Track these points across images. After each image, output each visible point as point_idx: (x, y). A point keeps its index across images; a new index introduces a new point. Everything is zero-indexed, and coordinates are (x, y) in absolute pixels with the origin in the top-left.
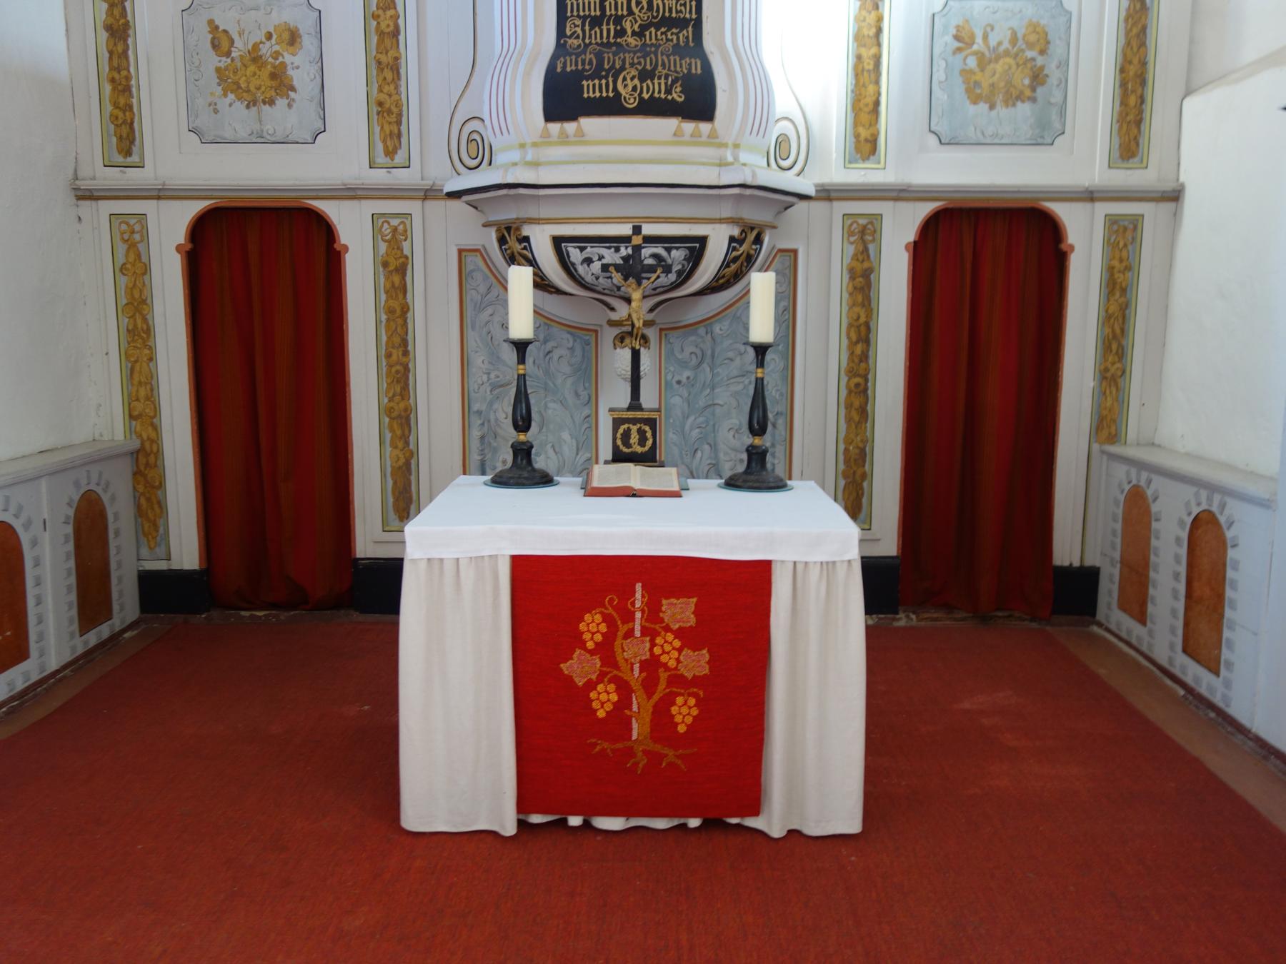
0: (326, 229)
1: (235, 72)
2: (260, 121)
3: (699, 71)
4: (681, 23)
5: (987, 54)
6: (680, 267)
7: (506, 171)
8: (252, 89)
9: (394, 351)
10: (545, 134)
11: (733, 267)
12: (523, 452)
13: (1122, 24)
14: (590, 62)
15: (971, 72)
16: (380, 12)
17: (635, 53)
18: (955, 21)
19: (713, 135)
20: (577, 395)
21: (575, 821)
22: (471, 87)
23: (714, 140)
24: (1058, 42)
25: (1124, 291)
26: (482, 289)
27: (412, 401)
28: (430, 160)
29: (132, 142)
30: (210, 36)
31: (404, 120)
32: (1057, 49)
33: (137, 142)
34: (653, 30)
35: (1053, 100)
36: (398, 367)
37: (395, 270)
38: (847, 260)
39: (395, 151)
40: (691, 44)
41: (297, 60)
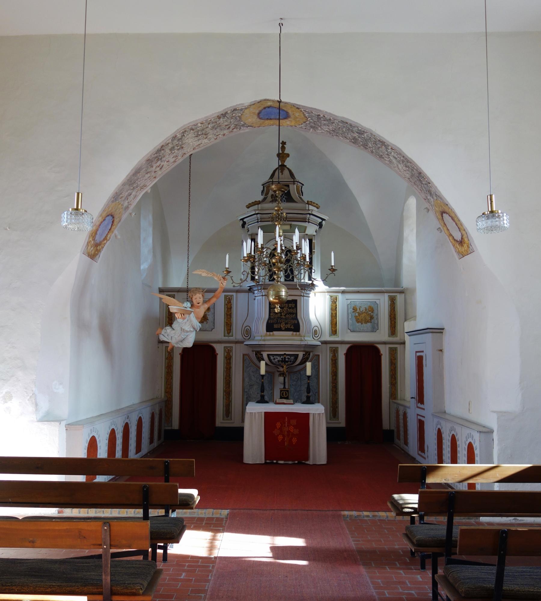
0: (213, 350)
4: (293, 314)
10: (266, 334)
12: (262, 397)
18: (353, 306)
19: (300, 334)
21: (275, 461)
23: (300, 335)
25: (394, 364)
28: (237, 335)
32: (375, 311)
37: (228, 359)
41: (209, 313)
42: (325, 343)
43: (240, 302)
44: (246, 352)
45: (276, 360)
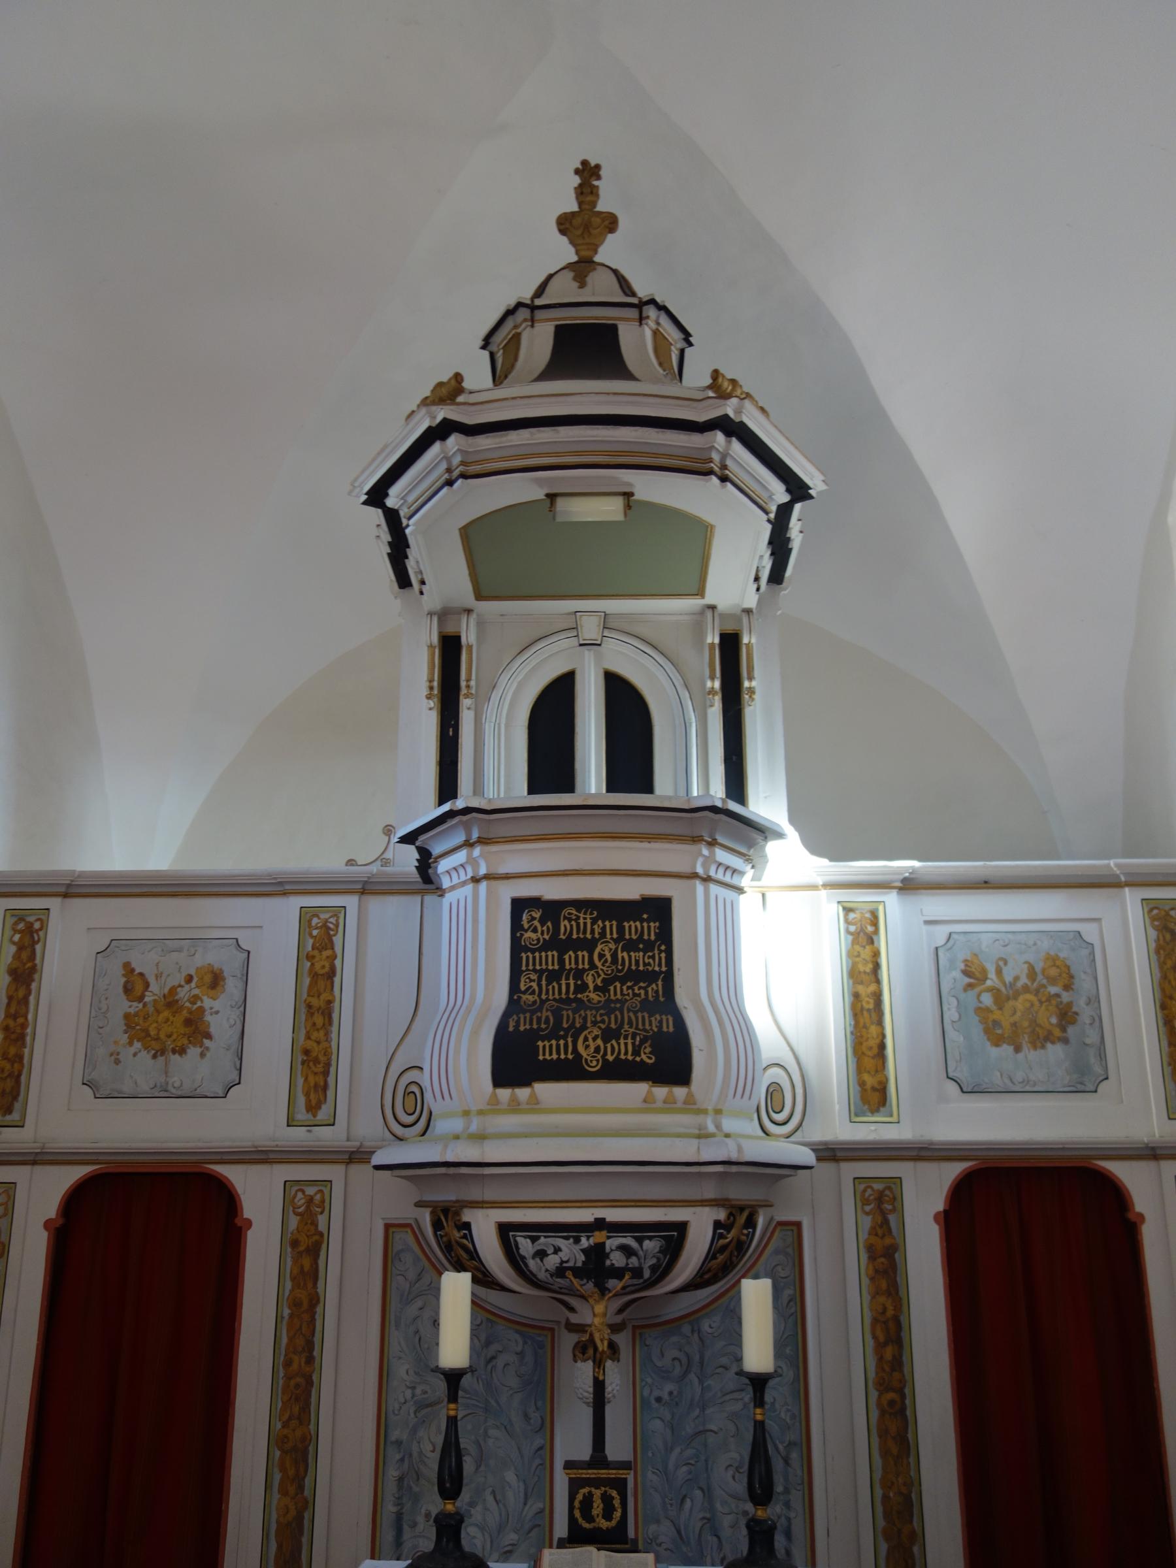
0: (225, 1199)
1: (145, 1019)
2: (166, 1073)
3: (671, 1029)
5: (1003, 989)
6: (654, 1261)
7: (446, 1147)
8: (162, 1036)
9: (296, 1358)
11: (721, 1258)
13: (1154, 957)
14: (547, 1021)
15: (988, 1010)
16: (316, 953)
17: (597, 1009)
18: (962, 955)
19: (690, 1100)
20: (526, 1416)
22: (419, 1013)
23: (690, 1106)
24: (1083, 976)
26: (412, 1275)
27: (312, 1427)
29: (15, 1097)
30: (123, 980)
31: (332, 1070)
32: (1083, 983)
33: (21, 1098)
34: (618, 984)
35: (1088, 1041)
36: (299, 1380)
37: (306, 1249)
38: (863, 1236)
39: (318, 1106)
40: (662, 999)
42: (830, 1153)
43: (378, 936)
44: (405, 1211)
45: (552, 1261)
